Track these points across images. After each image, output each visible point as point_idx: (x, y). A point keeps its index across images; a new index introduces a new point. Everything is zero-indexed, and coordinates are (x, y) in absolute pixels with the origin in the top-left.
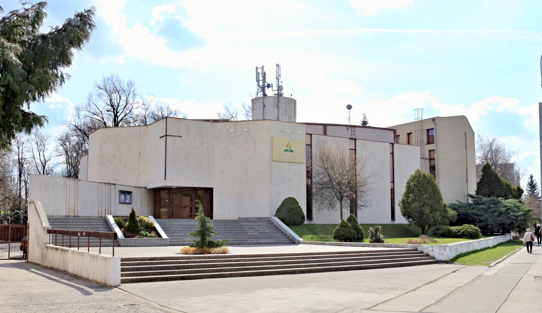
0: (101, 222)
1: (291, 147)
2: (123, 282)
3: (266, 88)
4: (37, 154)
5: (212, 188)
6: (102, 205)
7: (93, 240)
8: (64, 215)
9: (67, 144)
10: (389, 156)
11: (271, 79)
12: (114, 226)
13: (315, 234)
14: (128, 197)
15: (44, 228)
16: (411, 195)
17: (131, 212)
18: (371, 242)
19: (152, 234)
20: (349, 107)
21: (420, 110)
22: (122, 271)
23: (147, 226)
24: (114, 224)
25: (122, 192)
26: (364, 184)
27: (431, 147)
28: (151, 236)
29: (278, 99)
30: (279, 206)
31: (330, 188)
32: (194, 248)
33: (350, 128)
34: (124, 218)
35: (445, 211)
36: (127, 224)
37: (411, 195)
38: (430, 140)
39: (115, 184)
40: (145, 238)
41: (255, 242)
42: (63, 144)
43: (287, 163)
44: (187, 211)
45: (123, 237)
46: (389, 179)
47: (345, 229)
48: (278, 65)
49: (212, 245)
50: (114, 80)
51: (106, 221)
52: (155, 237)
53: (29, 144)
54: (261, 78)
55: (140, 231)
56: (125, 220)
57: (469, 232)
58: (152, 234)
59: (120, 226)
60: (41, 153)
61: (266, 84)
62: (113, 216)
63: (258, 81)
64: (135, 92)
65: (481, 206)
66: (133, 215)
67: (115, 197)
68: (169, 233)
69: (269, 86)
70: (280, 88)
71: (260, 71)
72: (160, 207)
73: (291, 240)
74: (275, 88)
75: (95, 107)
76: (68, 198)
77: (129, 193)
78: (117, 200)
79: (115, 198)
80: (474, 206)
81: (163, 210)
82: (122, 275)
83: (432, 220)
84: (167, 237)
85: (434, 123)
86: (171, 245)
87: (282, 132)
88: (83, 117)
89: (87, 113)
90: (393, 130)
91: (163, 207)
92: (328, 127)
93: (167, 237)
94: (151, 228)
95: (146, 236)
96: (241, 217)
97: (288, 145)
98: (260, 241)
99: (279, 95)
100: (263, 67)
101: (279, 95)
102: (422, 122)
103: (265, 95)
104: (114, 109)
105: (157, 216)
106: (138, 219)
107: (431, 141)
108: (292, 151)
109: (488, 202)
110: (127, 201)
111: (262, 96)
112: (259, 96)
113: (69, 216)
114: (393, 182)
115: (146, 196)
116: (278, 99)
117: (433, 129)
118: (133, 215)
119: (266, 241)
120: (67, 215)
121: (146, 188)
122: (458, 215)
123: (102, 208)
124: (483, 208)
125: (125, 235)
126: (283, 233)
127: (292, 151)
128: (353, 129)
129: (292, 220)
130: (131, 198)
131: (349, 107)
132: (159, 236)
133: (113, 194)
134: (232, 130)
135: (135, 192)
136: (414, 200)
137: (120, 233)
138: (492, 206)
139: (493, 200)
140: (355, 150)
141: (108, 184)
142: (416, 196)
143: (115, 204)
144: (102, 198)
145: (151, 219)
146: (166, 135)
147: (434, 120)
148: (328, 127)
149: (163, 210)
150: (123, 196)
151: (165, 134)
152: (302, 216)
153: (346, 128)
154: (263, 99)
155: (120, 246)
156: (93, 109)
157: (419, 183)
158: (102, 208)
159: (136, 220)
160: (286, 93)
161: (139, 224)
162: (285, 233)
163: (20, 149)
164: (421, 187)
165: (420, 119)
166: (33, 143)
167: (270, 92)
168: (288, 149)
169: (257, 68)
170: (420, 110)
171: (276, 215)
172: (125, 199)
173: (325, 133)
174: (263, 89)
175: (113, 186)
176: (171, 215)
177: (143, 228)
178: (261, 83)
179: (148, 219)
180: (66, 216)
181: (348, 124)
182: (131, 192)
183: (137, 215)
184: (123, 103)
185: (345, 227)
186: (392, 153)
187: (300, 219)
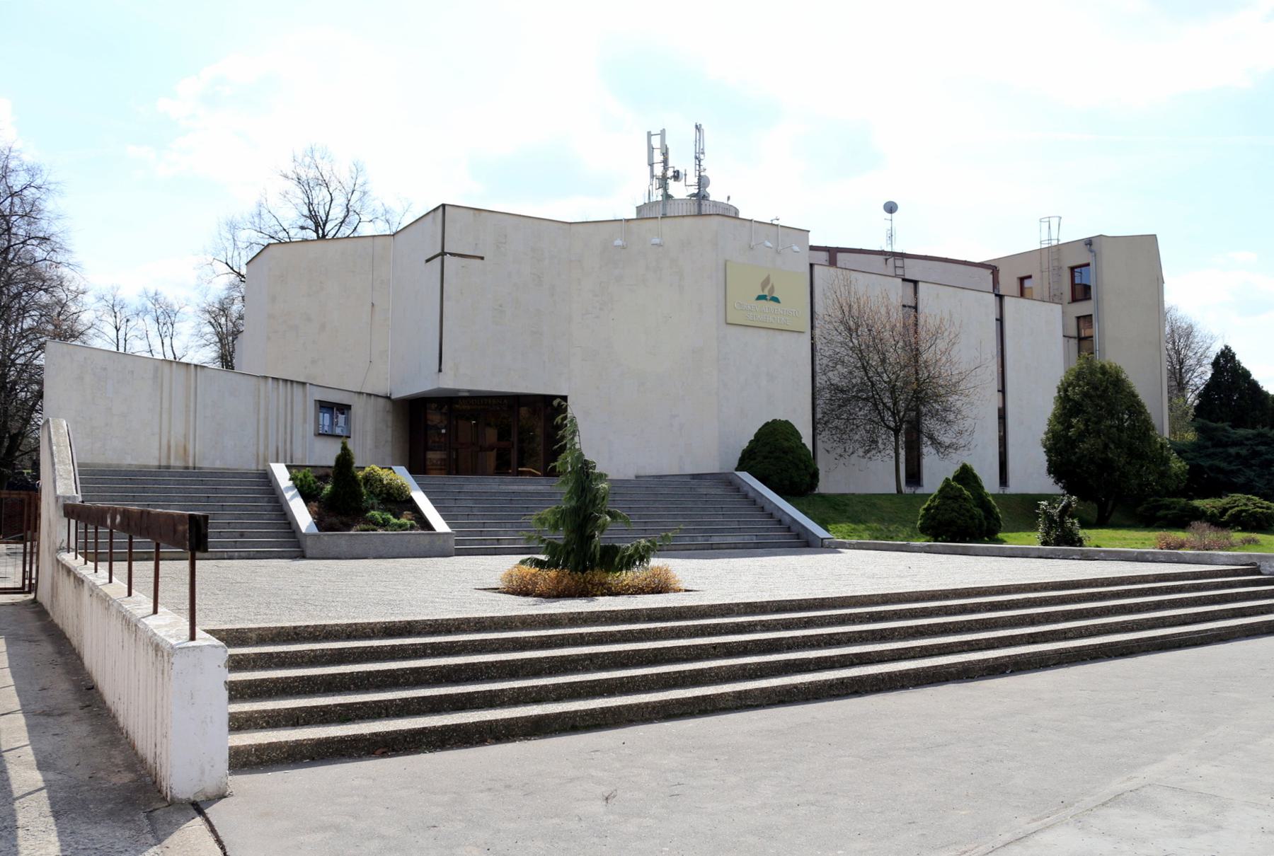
0: (252, 483)
1: (772, 289)
2: (243, 761)
3: (671, 182)
4: (156, 344)
5: (1149, 242)
6: (266, 436)
7: (143, 543)
8: (156, 463)
9: (223, 320)
10: (993, 326)
11: (681, 160)
12: (288, 495)
13: (859, 522)
14: (341, 418)
15: (57, 498)
16: (1074, 421)
17: (339, 452)
18: (1045, 543)
19: (403, 520)
20: (891, 208)
21: (1054, 222)
22: (232, 699)
23: (389, 494)
24: (288, 489)
25: (324, 406)
26: (953, 388)
27: (1083, 308)
28: (401, 527)
29: (700, 205)
30: (745, 444)
31: (867, 399)
32: (553, 573)
33: (891, 260)
34: (321, 472)
35: (1166, 461)
36: (328, 487)
37: (1074, 421)
38: (1081, 292)
39: (304, 384)
40: (380, 532)
41: (700, 541)
42: (215, 324)
43: (763, 332)
44: (491, 459)
45: (315, 530)
46: (995, 385)
47: (956, 506)
48: (698, 128)
49: (613, 559)
50: (317, 156)
51: (267, 479)
52: (412, 527)
53: (140, 321)
54: (658, 157)
55: (367, 510)
56: (323, 478)
57: (1253, 515)
58: (403, 520)
59: (308, 495)
60: (167, 341)
61: (670, 173)
62: (288, 467)
63: (651, 165)
64: (367, 188)
65: (1232, 450)
66: (345, 460)
67: (305, 418)
68: (455, 517)
69: (677, 176)
70: (702, 182)
71: (656, 142)
72: (427, 449)
73: (798, 536)
74: (693, 179)
75: (274, 222)
76: (165, 416)
77: (344, 408)
78: (310, 428)
79: (305, 421)
80: (1211, 450)
81: (433, 456)
82: (239, 724)
83: (1134, 482)
84: (449, 530)
85: (1091, 251)
86: (459, 553)
87: (751, 248)
88: (244, 245)
89: (255, 236)
90: (992, 268)
91: (432, 450)
92: (840, 256)
93: (449, 530)
94: (400, 502)
95: (385, 524)
96: (642, 473)
97: (766, 282)
98: (716, 540)
99: (700, 197)
100: (663, 134)
101: (700, 197)
102: (1059, 249)
103: (667, 197)
104: (317, 225)
105: (417, 468)
106: (360, 474)
107: (1078, 296)
108: (776, 300)
109: (1248, 439)
110: (338, 431)
111: (660, 198)
112: (653, 199)
113: (168, 467)
114: (1003, 391)
115: (390, 418)
116: (700, 205)
117: (1088, 265)
118: (345, 460)
119: (730, 540)
120: (164, 463)
121: (388, 398)
122: (1190, 472)
123: (266, 447)
124: (1238, 454)
125: (321, 523)
126: (771, 515)
127: (776, 300)
128: (899, 263)
129: (787, 482)
130: (347, 422)
131: (891, 208)
132: (426, 525)
133: (298, 409)
134: (618, 242)
135: (360, 409)
136: (1081, 436)
137: (303, 516)
138: (1262, 448)
139: (1260, 435)
140: (916, 308)
141: (286, 381)
142: (1088, 420)
143: (304, 437)
144: (267, 419)
145: (401, 476)
146: (443, 254)
147: (1089, 242)
148: (840, 256)
149: (433, 456)
150: (327, 416)
151: (439, 251)
152: (811, 471)
153: (882, 258)
154: (664, 206)
155: (303, 556)
156: (270, 225)
157: (1096, 389)
158: (266, 447)
159: (354, 478)
160: (716, 193)
161: (363, 490)
162: (777, 515)
163: (122, 333)
164: (1100, 397)
165: (1055, 243)
166: (149, 319)
167: (679, 191)
168: (766, 293)
169: (650, 135)
170: (1054, 222)
171: (741, 467)
172: (333, 423)
173: (832, 262)
174: (664, 179)
175: (298, 390)
176: (453, 467)
177: (375, 501)
178: (658, 170)
179: (392, 476)
180: (160, 467)
181: (888, 249)
182: (348, 407)
183: (357, 463)
184: (337, 213)
185: (955, 498)
186: (1001, 320)
187: (808, 479)
